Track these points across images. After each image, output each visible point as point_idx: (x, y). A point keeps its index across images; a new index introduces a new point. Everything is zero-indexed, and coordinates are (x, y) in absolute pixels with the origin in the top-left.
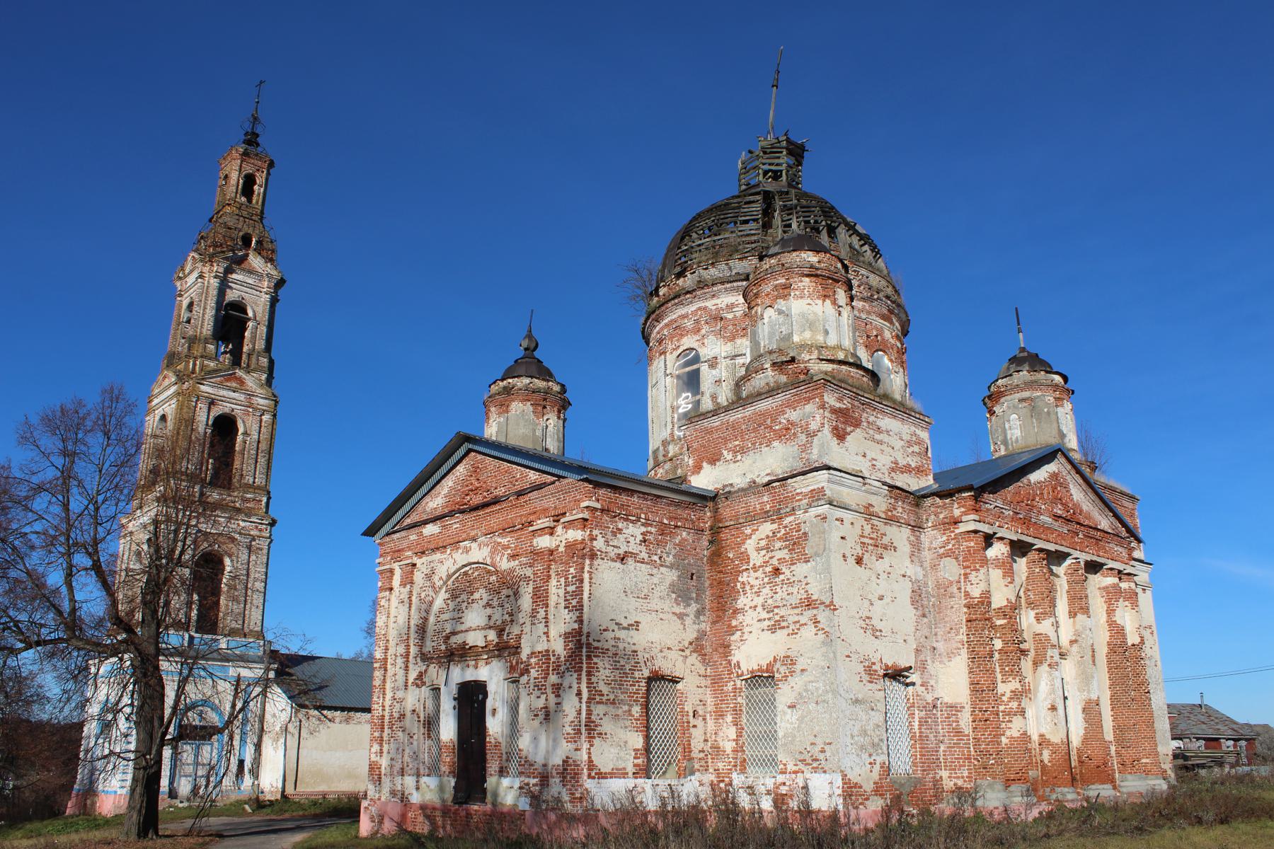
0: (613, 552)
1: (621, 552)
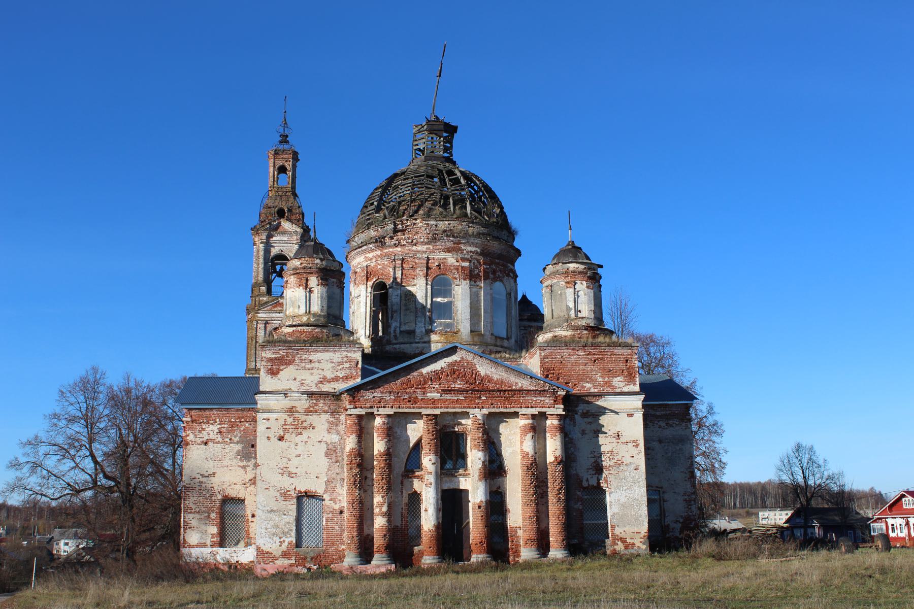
0: (199, 440)
1: (205, 440)
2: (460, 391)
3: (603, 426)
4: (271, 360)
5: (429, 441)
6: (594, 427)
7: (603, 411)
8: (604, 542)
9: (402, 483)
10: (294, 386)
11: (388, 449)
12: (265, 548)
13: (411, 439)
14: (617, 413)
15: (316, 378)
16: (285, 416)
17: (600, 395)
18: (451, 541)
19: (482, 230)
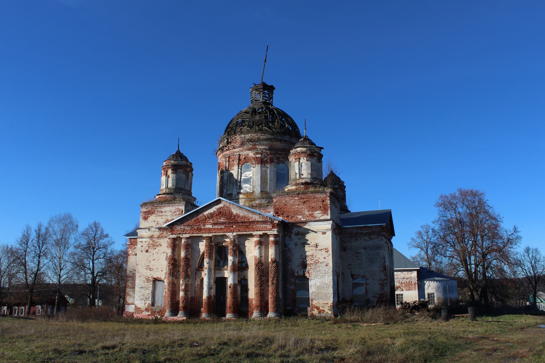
0: (133, 253)
2: (222, 224)
4: (145, 212)
6: (302, 241)
7: (307, 231)
9: (196, 274)
10: (154, 225)
12: (139, 306)
15: (164, 220)
16: (148, 240)
17: (305, 222)
19: (269, 136)
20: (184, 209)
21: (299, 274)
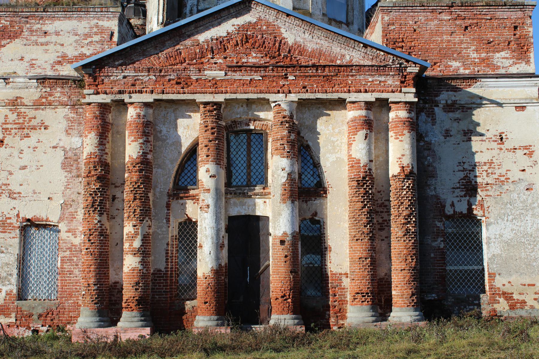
2: (256, 67)
3: (478, 124)
5: (206, 142)
6: (463, 125)
7: (478, 102)
8: (479, 299)
9: (168, 206)
10: (21, 68)
11: (145, 154)
13: (183, 141)
14: (500, 105)
15: (53, 57)
17: (473, 78)
18: (239, 293)
20: (116, 30)
21: (458, 209)
